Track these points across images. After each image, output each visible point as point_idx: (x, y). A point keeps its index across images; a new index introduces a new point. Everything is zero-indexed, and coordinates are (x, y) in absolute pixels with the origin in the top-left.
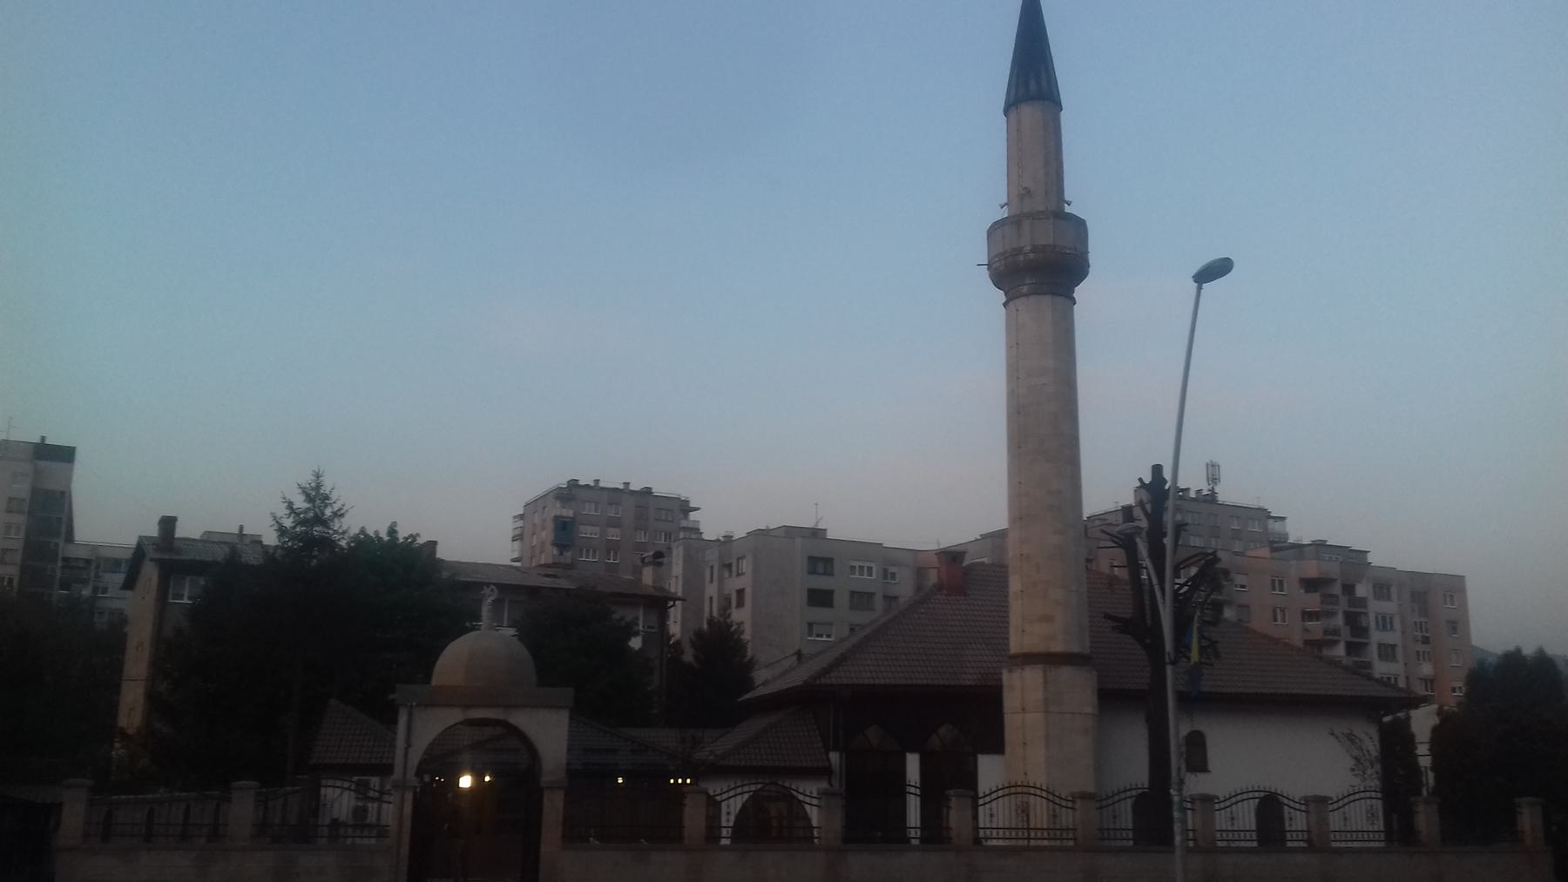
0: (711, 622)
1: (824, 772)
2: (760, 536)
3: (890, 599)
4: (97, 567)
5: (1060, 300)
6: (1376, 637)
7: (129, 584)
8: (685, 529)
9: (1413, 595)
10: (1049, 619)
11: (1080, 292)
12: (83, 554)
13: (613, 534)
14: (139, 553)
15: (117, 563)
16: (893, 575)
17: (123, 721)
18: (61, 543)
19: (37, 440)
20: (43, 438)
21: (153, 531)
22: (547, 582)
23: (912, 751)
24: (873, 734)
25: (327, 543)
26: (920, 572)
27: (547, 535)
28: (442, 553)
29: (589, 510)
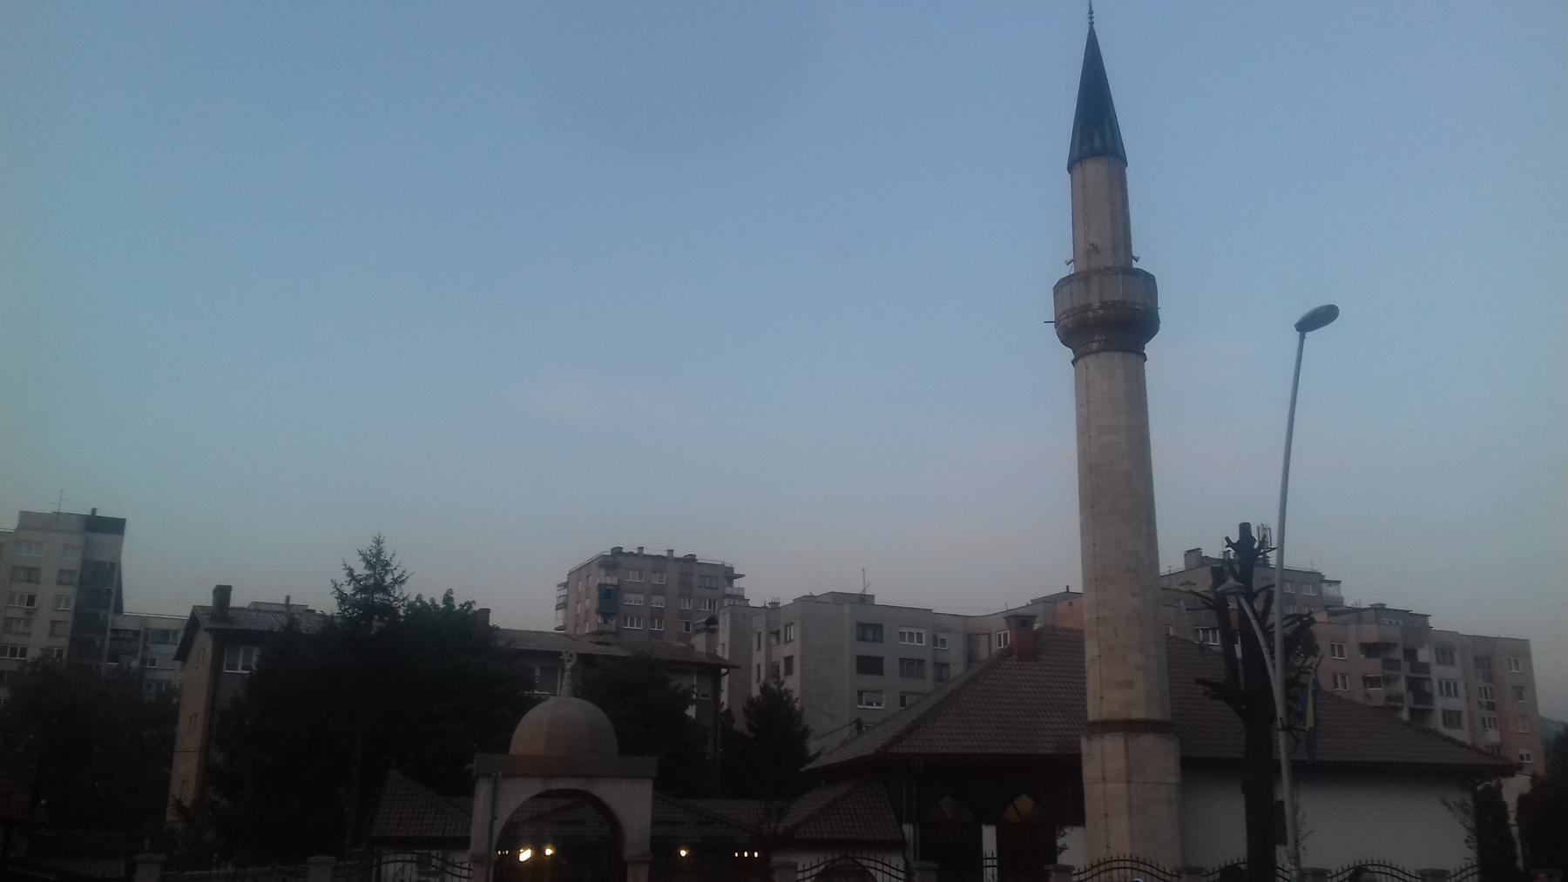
0: (765, 689)
1: (899, 845)
2: (807, 601)
3: (942, 666)
4: (146, 638)
5: (1132, 357)
6: (1440, 703)
7: (183, 655)
8: (729, 596)
9: (1476, 659)
10: (1129, 684)
11: (1149, 348)
12: (134, 626)
13: (658, 602)
14: (193, 623)
15: (164, 635)
16: (943, 641)
17: (175, 791)
18: (110, 616)
19: (88, 512)
20: (94, 511)
21: (208, 601)
22: (601, 650)
23: (988, 824)
24: (1025, 803)
25: (387, 610)
26: (971, 638)
27: (591, 603)
28: (494, 620)
29: (633, 577)
